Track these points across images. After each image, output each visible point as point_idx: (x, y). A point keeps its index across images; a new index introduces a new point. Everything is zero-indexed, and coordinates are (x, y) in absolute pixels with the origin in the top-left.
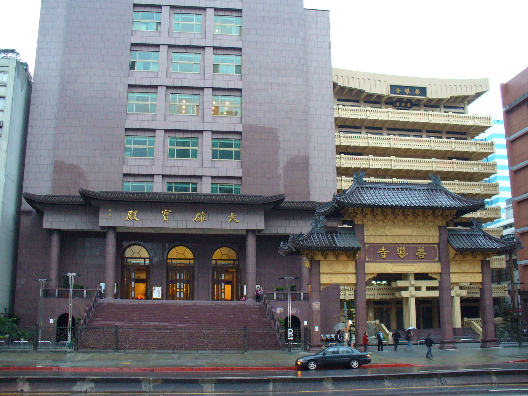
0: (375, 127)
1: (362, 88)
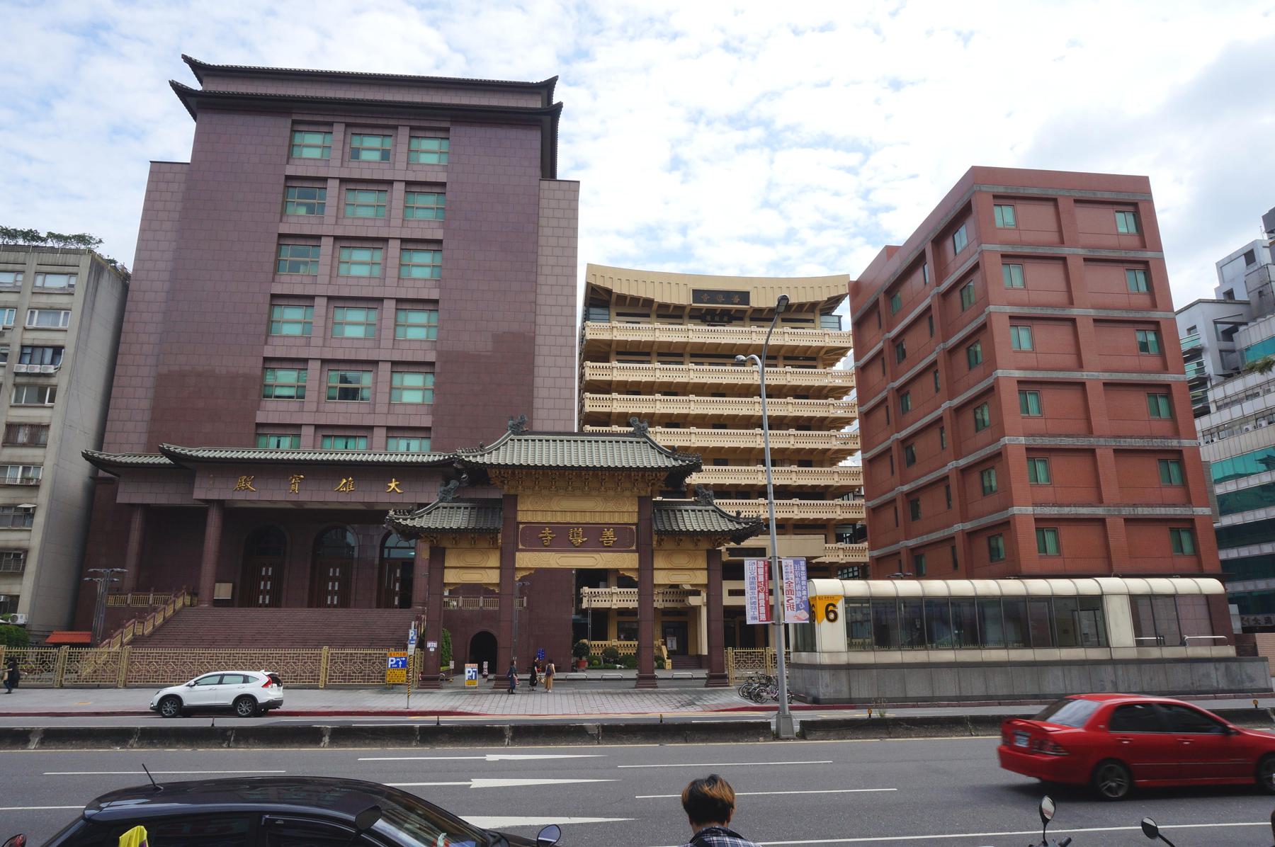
0: (671, 353)
1: (650, 296)
